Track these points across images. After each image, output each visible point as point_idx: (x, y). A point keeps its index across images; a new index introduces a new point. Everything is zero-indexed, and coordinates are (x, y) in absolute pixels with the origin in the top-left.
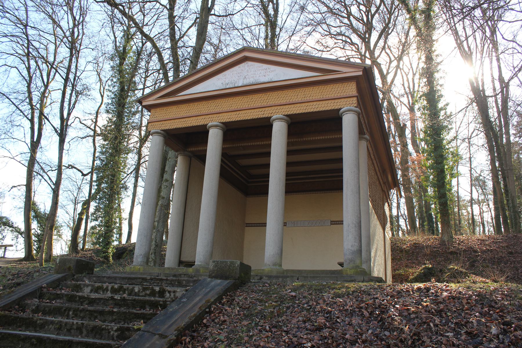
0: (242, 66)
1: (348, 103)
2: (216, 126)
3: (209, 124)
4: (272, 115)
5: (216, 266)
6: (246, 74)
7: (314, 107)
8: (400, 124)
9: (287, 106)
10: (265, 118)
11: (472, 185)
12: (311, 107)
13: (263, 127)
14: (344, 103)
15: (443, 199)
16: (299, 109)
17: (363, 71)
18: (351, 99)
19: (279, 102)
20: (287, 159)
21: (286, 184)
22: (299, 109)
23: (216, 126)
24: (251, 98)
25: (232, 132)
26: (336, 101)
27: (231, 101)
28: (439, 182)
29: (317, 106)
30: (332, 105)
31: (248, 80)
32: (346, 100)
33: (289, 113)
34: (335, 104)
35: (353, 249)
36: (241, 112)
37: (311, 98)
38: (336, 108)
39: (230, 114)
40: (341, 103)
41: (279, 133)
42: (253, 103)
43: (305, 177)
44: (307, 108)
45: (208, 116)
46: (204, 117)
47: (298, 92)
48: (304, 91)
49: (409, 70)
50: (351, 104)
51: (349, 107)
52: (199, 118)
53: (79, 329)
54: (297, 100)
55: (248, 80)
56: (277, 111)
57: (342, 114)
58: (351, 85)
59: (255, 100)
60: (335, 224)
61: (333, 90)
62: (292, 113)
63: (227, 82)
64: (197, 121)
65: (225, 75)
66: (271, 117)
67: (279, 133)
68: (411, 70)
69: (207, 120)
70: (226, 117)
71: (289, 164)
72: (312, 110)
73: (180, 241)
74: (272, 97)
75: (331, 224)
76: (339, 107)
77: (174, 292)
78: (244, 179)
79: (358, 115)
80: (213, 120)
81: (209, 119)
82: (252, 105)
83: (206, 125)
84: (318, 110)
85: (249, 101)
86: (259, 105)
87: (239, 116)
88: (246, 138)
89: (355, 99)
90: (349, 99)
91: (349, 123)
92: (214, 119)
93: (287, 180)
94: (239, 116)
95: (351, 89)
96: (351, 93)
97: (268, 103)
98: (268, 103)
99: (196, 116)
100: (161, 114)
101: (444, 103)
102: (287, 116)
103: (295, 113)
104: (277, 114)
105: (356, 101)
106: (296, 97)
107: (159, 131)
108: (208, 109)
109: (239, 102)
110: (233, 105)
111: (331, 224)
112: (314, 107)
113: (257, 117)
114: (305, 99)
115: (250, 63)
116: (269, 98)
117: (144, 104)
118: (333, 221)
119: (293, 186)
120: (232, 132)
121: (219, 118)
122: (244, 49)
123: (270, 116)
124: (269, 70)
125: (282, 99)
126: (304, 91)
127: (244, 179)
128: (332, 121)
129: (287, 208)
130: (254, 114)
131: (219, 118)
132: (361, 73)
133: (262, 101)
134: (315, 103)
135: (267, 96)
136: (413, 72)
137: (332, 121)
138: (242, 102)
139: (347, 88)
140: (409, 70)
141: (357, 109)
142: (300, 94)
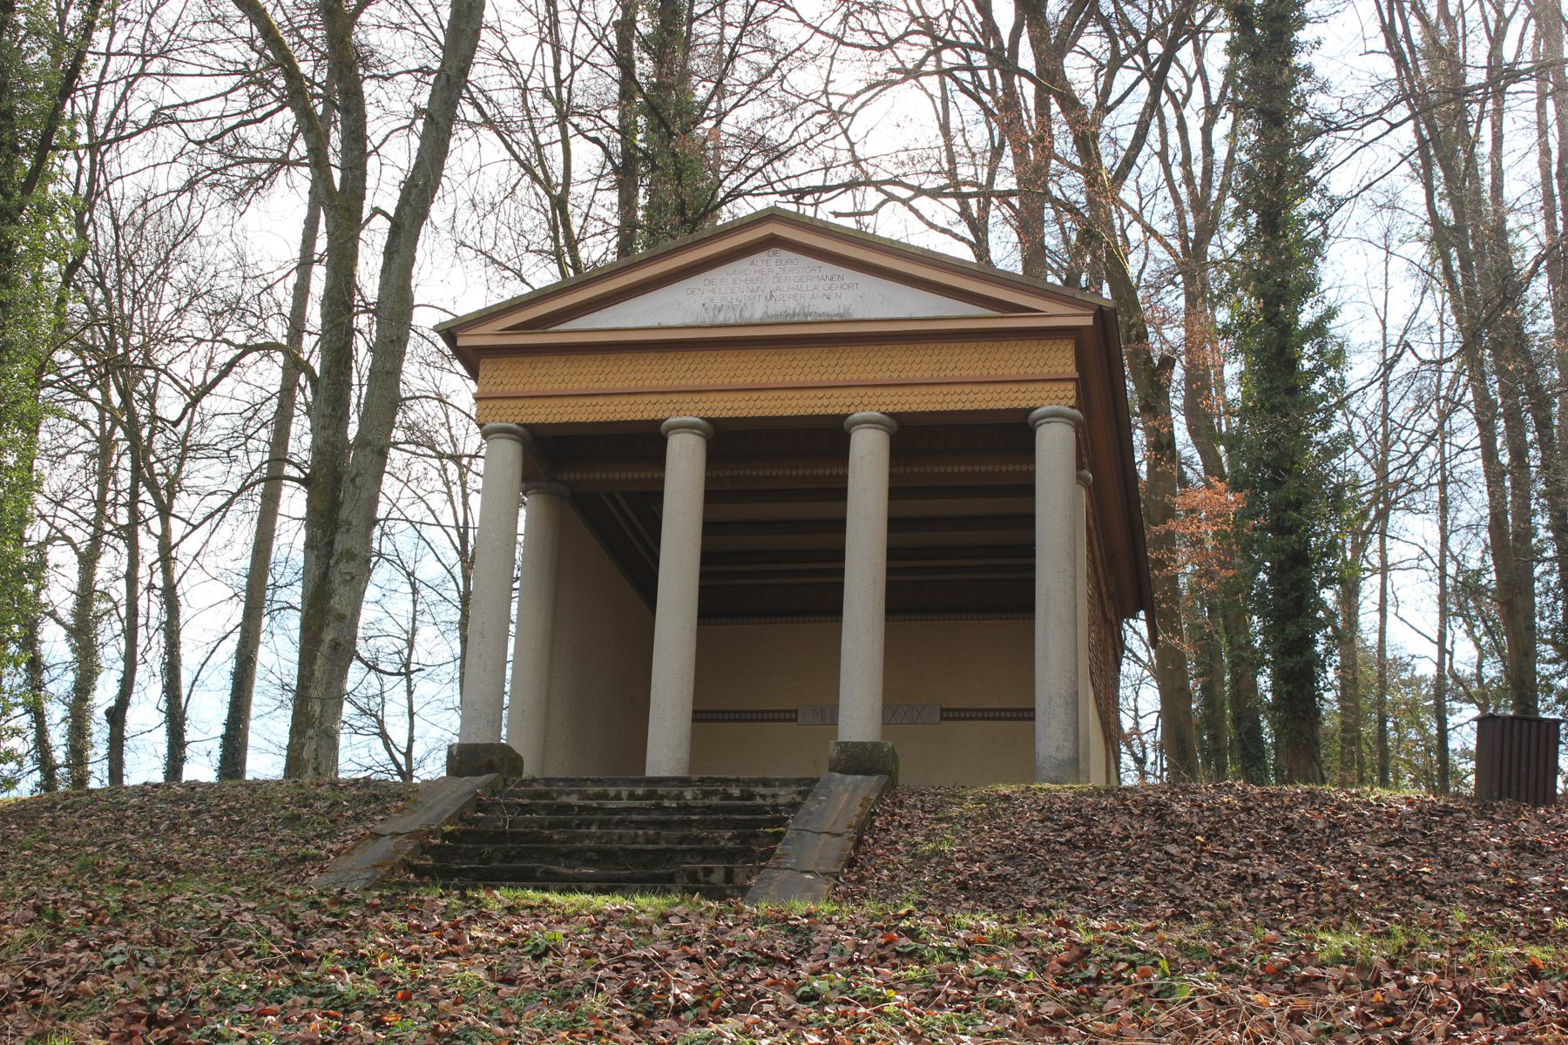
0: (760, 258)
1: (1052, 395)
2: (690, 427)
3: (671, 420)
4: (852, 409)
5: (843, 752)
6: (774, 286)
8: (1150, 360)
9: (892, 391)
10: (830, 416)
11: (1444, 614)
12: (956, 398)
13: (828, 439)
14: (1044, 395)
15: (1297, 658)
17: (1095, 316)
18: (1062, 386)
19: (871, 377)
23: (690, 427)
26: (1023, 387)
28: (1284, 596)
29: (972, 397)
31: (780, 303)
32: (1048, 386)
33: (898, 409)
34: (1020, 396)
35: (1060, 755)
36: (763, 395)
37: (956, 373)
38: (1024, 404)
41: (868, 457)
45: (668, 398)
46: (654, 398)
49: (1190, 81)
50: (1062, 399)
51: (1055, 407)
52: (639, 399)
55: (780, 303)
60: (954, 719)
62: (906, 408)
63: (718, 301)
65: (711, 282)
66: (847, 416)
67: (868, 457)
68: (1197, 85)
70: (721, 406)
72: (960, 407)
75: (942, 719)
77: (774, 796)
78: (770, 577)
79: (1078, 426)
81: (671, 406)
83: (662, 421)
89: (1071, 386)
90: (1055, 386)
91: (1054, 449)
92: (685, 406)
95: (1063, 360)
96: (1060, 370)
97: (841, 377)
98: (841, 377)
99: (629, 394)
100: (510, 377)
101: (1319, 310)
102: (892, 415)
104: (867, 405)
105: (1073, 393)
106: (916, 367)
107: (513, 426)
108: (667, 375)
110: (739, 373)
111: (942, 719)
114: (942, 374)
115: (785, 255)
117: (462, 342)
118: (948, 710)
121: (700, 406)
123: (845, 411)
124: (839, 283)
127: (770, 577)
129: (897, 656)
132: (1089, 321)
133: (822, 370)
134: (967, 389)
136: (1207, 97)
140: (1190, 81)
141: (1076, 412)
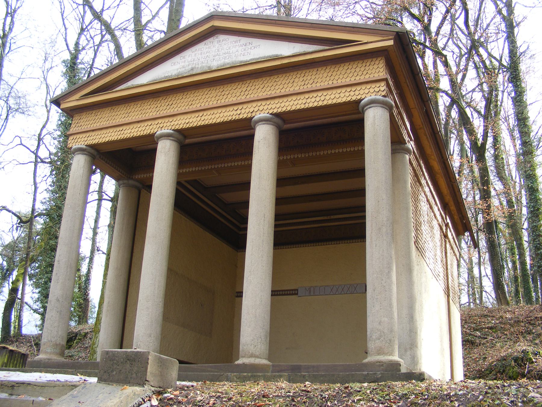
7: (318, 99)
14: (367, 91)
16: (296, 103)
20: (277, 192)
21: (275, 232)
22: (296, 103)
24: (221, 90)
25: (195, 147)
27: (192, 96)
30: (347, 94)
33: (94, 142)
38: (354, 98)
39: (189, 116)
40: (362, 92)
42: (225, 97)
43: (325, 218)
44: (308, 101)
46: (149, 123)
47: (294, 77)
48: (303, 75)
53: (425, 178)
54: (292, 89)
56: (261, 108)
57: (363, 108)
58: (377, 62)
59: (227, 93)
61: (349, 71)
64: (140, 129)
66: (360, 100)
69: (155, 126)
71: (280, 201)
73: (121, 320)
74: (253, 87)
75: (297, 290)
76: (359, 97)
80: (160, 123)
81: (158, 126)
82: (223, 101)
84: (325, 103)
85: (219, 95)
86: (234, 100)
87: (202, 119)
88: (216, 156)
91: (376, 123)
93: (276, 226)
94: (203, 118)
103: (289, 109)
106: (290, 85)
107: (84, 147)
109: (203, 97)
110: (193, 103)
111: (297, 290)
112: (318, 99)
113: (230, 118)
115: (222, 37)
116: (248, 89)
119: (285, 237)
120: (195, 147)
121: (172, 124)
122: (211, 17)
123: (249, 115)
125: (269, 88)
126: (303, 75)
128: (343, 127)
130: (225, 114)
131: (172, 124)
132: (391, 43)
135: (247, 85)
137: (343, 127)
138: (207, 96)
139: (371, 67)
142: (296, 80)
